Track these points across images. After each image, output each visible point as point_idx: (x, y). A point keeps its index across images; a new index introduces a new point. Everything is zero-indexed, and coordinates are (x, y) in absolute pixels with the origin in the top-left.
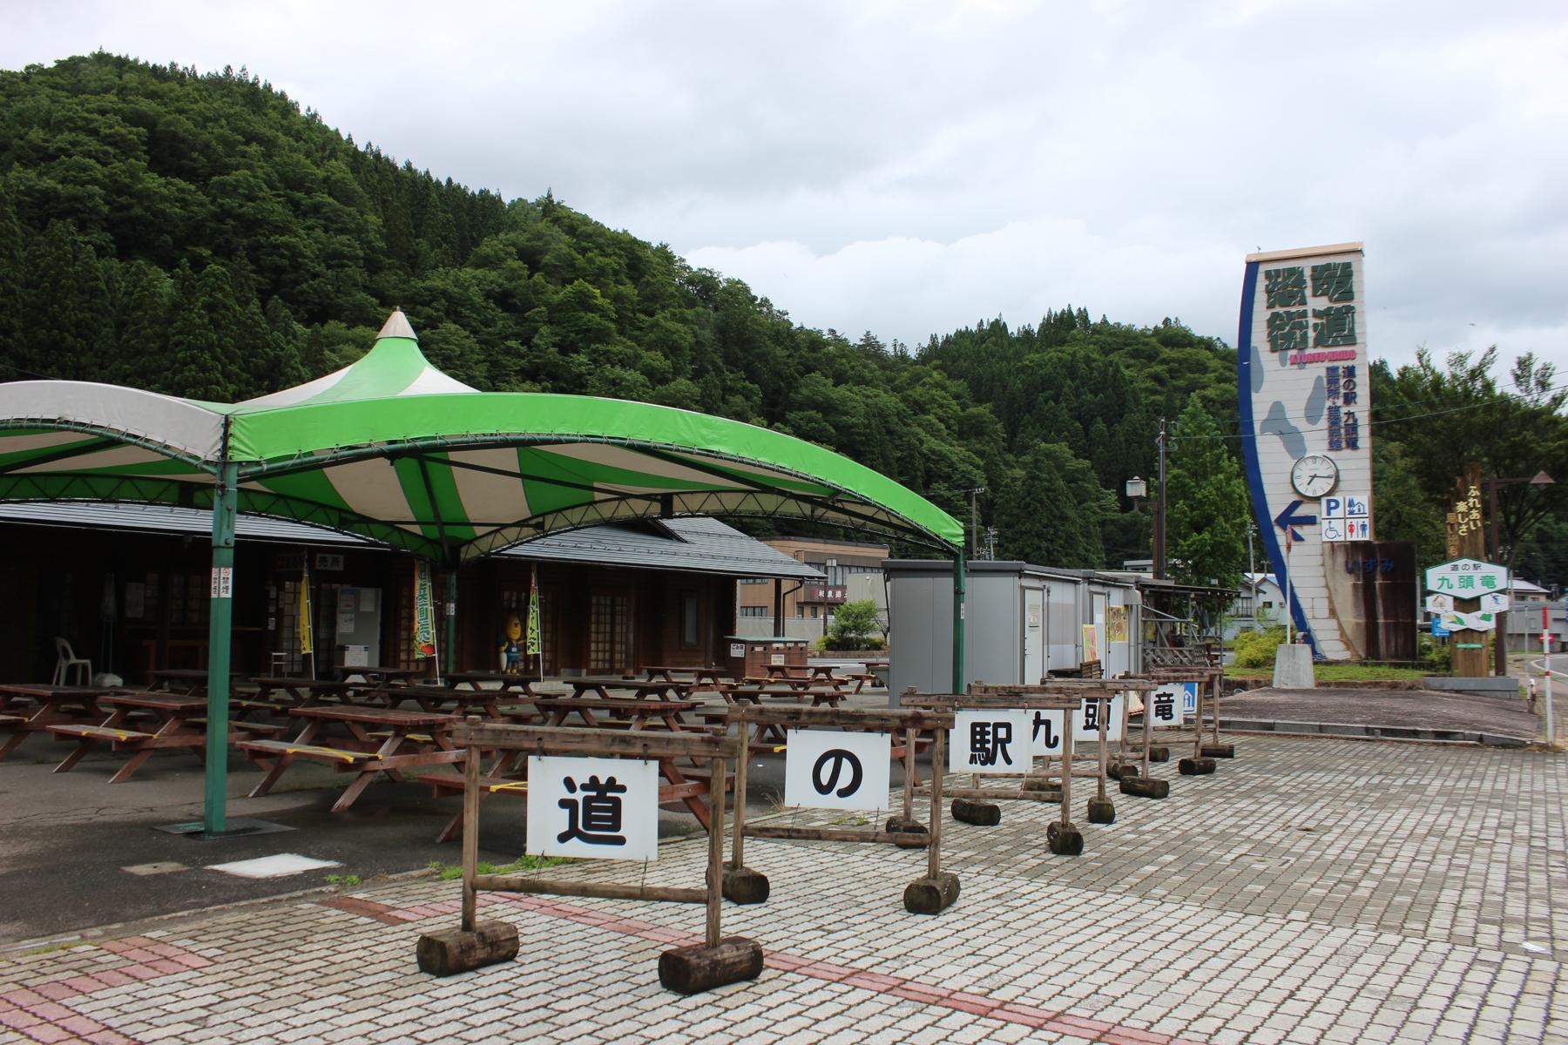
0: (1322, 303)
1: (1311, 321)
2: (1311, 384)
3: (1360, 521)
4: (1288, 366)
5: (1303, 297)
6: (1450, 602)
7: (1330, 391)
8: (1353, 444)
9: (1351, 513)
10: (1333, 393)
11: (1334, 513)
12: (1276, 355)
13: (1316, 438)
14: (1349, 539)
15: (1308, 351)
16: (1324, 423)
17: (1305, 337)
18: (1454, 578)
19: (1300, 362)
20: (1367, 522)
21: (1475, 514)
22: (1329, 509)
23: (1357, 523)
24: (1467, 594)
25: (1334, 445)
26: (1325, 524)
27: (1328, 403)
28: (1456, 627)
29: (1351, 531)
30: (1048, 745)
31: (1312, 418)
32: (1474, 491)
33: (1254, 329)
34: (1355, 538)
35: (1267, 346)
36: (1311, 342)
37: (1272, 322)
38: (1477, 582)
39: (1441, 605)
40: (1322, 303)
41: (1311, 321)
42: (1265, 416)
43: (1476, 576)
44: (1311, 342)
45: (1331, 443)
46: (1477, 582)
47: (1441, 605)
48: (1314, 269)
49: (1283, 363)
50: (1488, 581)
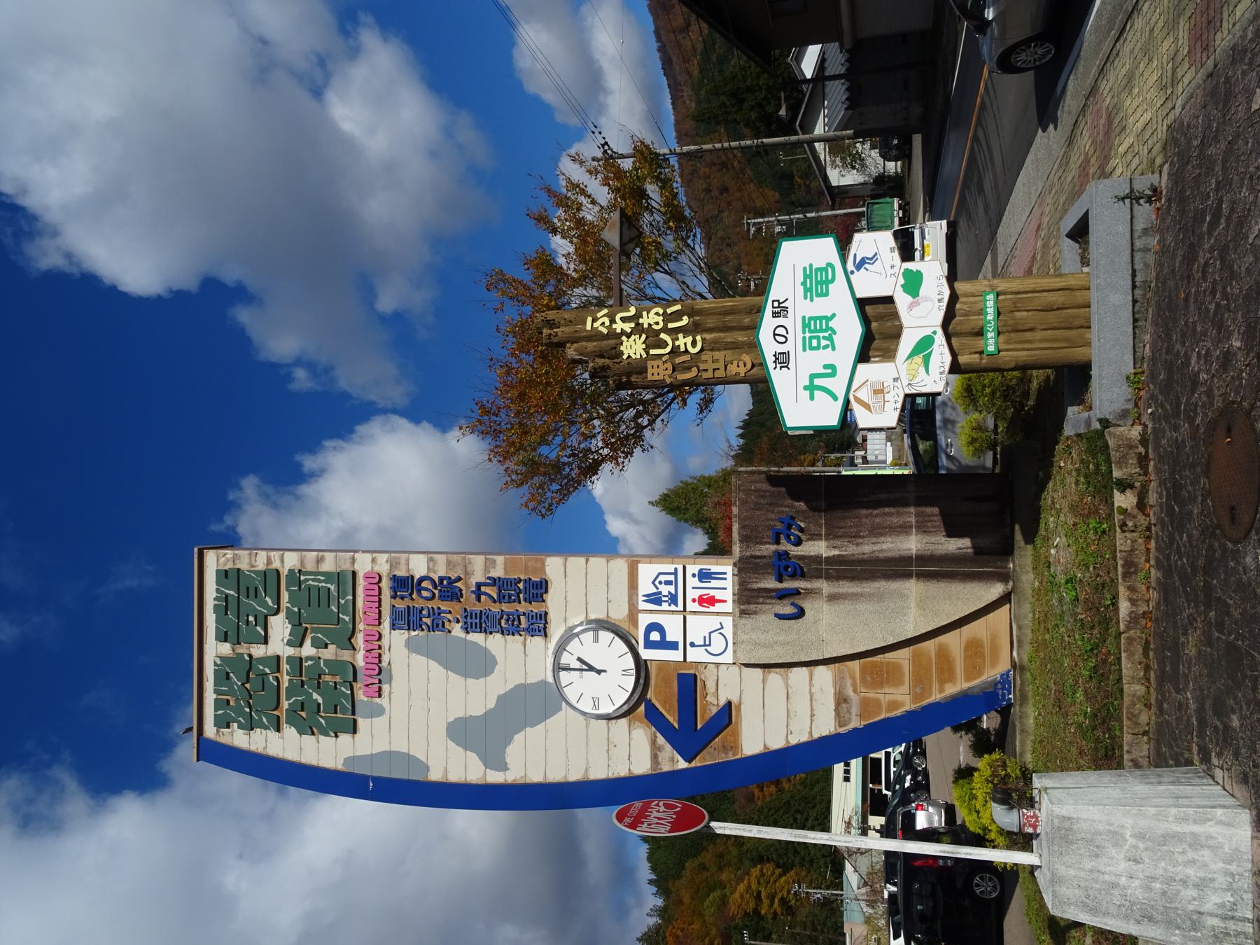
0: (280, 627)
1: (308, 650)
2: (419, 661)
3: (692, 582)
4: (384, 701)
5: (265, 660)
6: (873, 371)
7: (433, 628)
8: (539, 589)
9: (673, 599)
10: (438, 625)
11: (673, 634)
12: (362, 723)
13: (517, 660)
14: (728, 607)
15: (360, 661)
16: (494, 642)
17: (336, 666)
18: (807, 362)
19: (379, 673)
20: (693, 569)
21: (652, 318)
22: (664, 644)
23: (694, 589)
24: (850, 331)
25: (539, 626)
26: (695, 655)
27: (457, 630)
28: (941, 356)
29: (712, 601)
30: (833, 374)
31: (483, 665)
32: (599, 322)
33: (291, 755)
34: (728, 595)
35: (345, 738)
36: (346, 655)
37: (307, 728)
38: (819, 307)
39: (879, 391)
40: (280, 627)
41: (308, 650)
42: (473, 758)
43: (802, 308)
44: (346, 655)
45: (532, 632)
46: (819, 307)
47: (879, 391)
48: (223, 637)
49: (380, 711)
50: (816, 282)
